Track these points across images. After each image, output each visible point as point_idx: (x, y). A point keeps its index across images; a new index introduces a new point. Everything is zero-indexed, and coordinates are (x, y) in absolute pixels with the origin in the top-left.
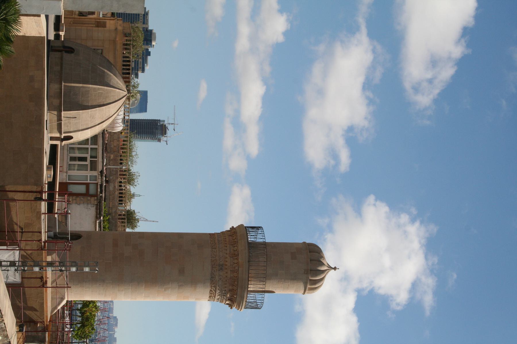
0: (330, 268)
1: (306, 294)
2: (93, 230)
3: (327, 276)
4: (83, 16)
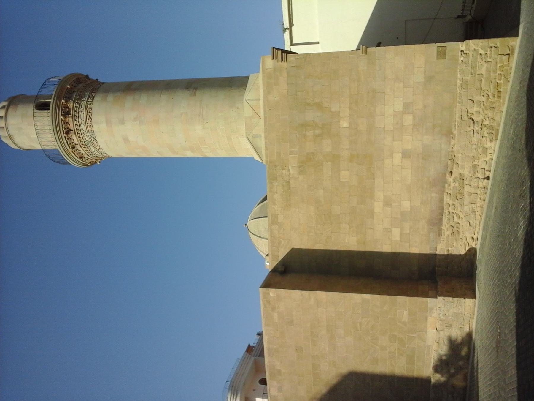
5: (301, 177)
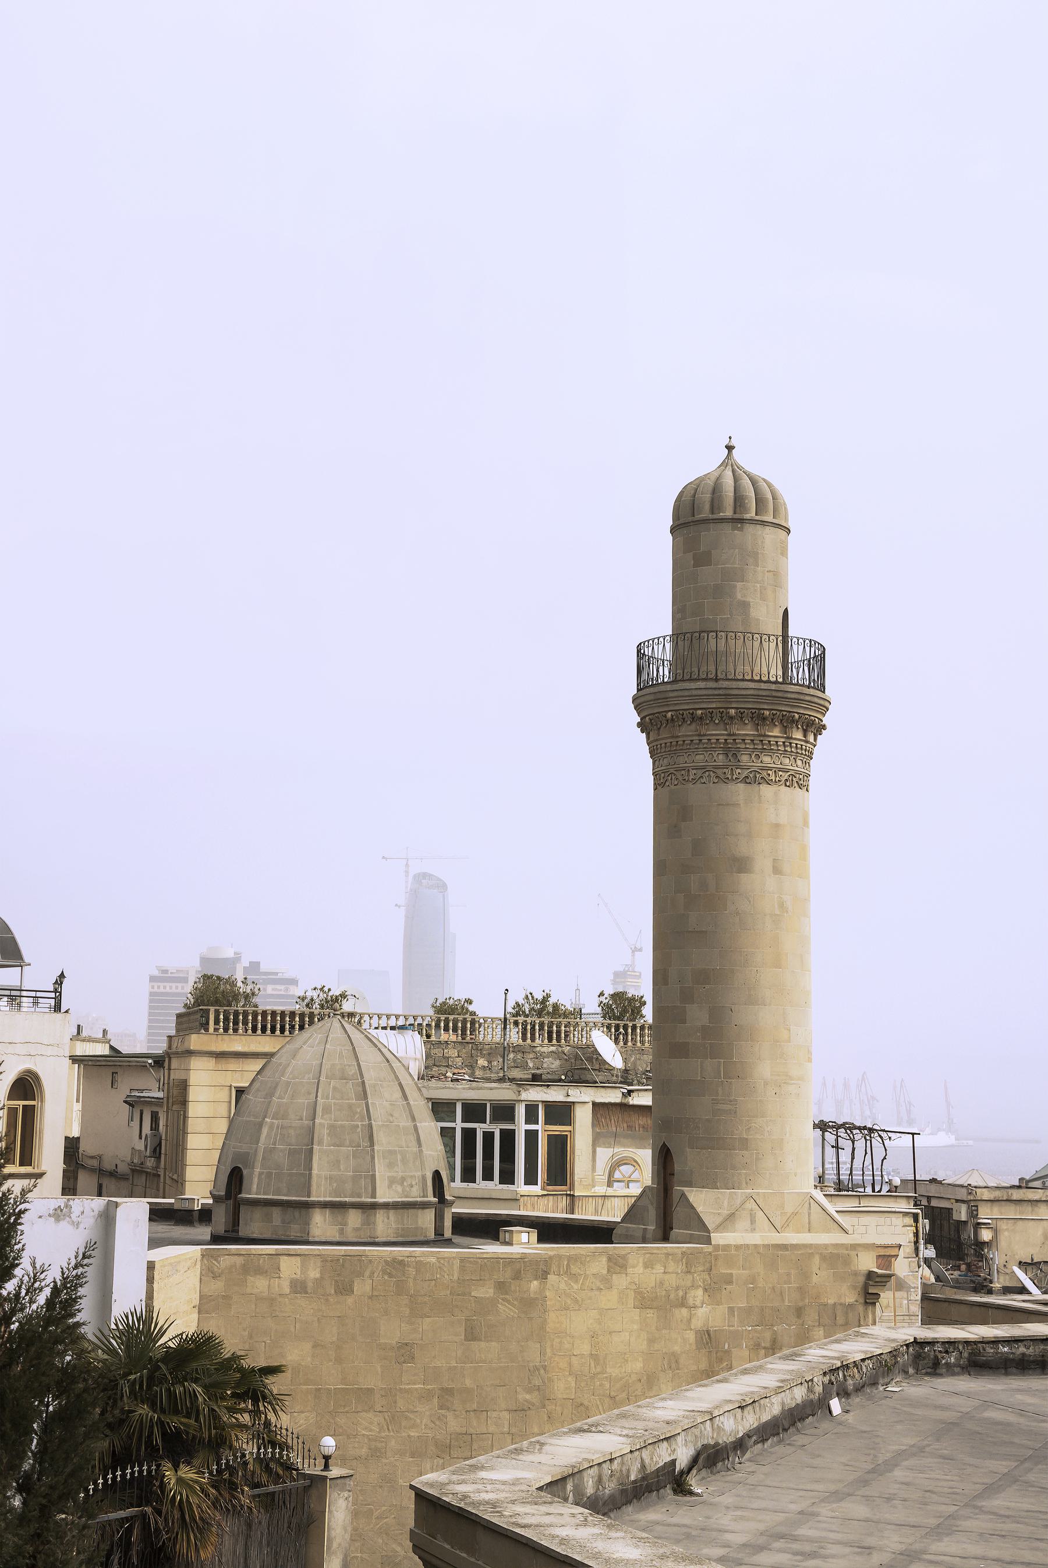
0: (728, 460)
1: (791, 525)
2: (651, 1094)
3: (747, 468)
4: (160, 1144)
5: (691, 1336)
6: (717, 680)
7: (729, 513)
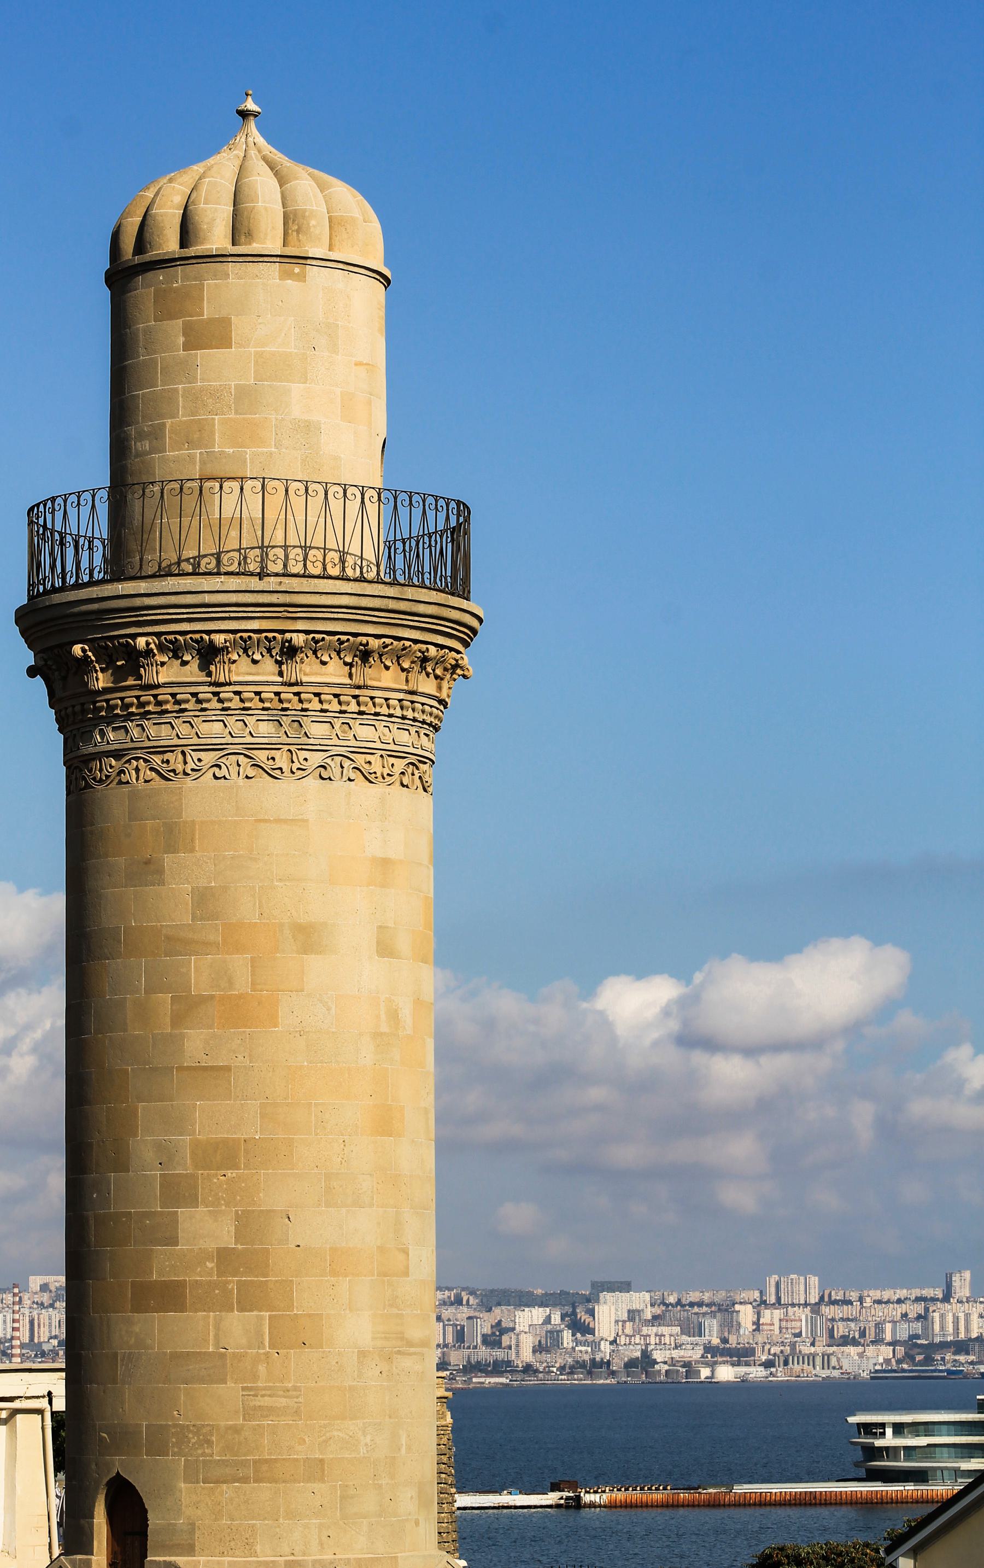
2: (63, 1374)
6: (261, 575)
7: (273, 245)
